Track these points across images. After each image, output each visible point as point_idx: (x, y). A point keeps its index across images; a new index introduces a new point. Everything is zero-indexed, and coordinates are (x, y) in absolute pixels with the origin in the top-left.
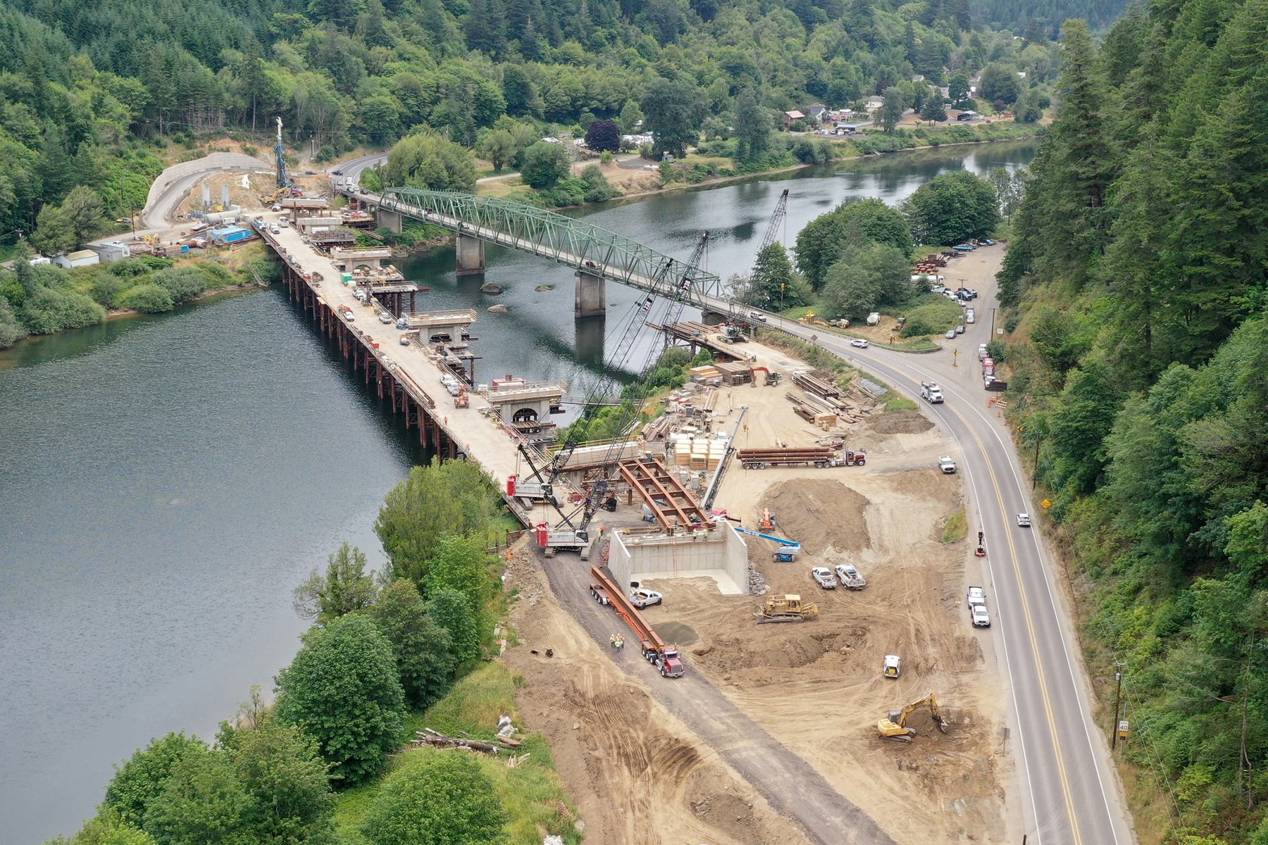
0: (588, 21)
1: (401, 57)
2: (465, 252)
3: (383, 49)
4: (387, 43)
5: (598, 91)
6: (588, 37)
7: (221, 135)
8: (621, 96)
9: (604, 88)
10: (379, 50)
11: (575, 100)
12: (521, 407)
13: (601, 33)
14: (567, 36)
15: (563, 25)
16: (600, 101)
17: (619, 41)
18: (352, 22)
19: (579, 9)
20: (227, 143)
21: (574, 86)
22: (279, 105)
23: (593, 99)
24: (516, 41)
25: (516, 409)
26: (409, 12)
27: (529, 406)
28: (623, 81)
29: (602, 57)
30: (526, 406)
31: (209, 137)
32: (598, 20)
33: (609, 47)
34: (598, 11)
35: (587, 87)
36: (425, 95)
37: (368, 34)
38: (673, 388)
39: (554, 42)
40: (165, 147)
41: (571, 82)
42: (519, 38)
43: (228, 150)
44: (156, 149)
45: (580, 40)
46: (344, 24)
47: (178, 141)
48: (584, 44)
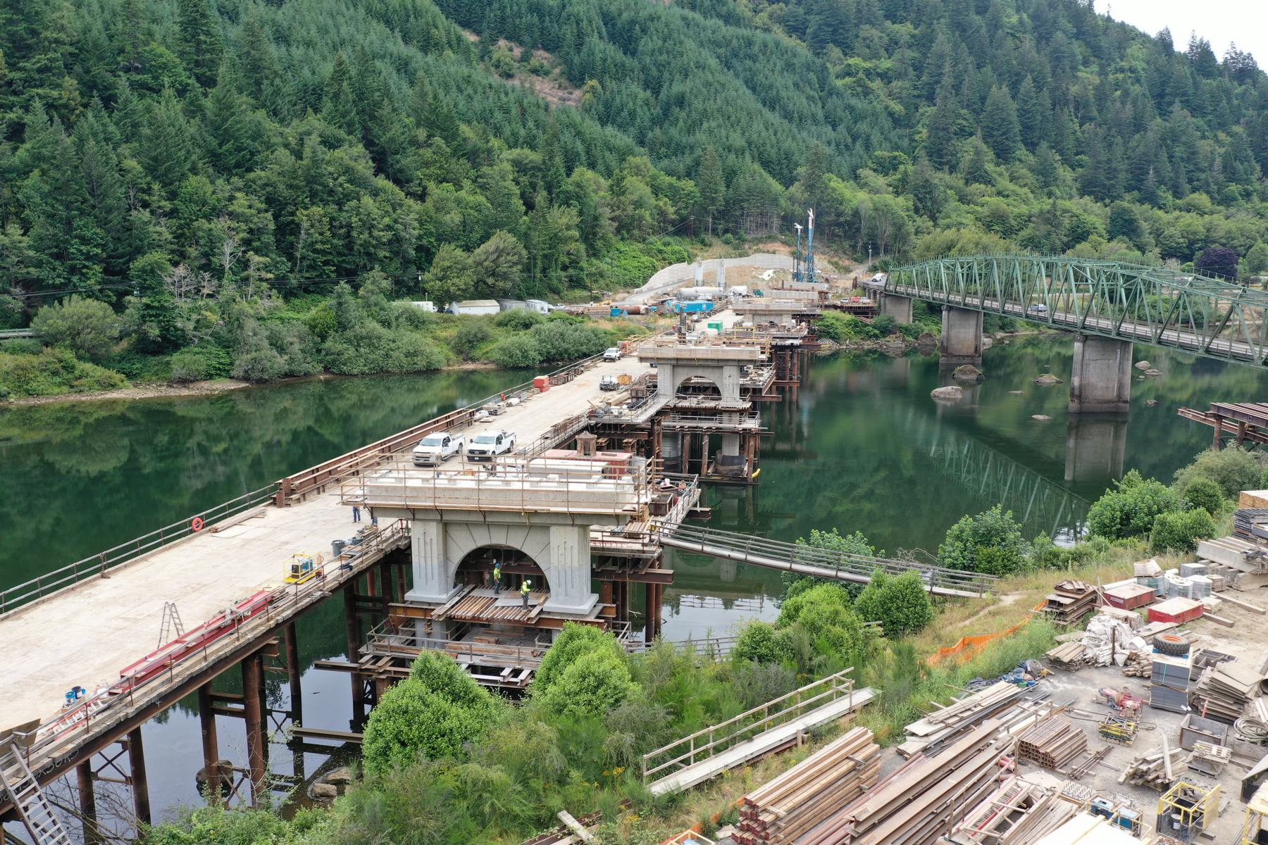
0: (1221, 177)
1: (999, 193)
2: (953, 333)
3: (983, 186)
4: (989, 182)
5: (1222, 233)
6: (1218, 192)
7: (771, 239)
8: (1248, 242)
9: (1229, 232)
10: (977, 187)
11: (1191, 243)
12: (482, 539)
13: (1234, 188)
14: (1194, 190)
15: (1190, 181)
16: (1224, 245)
17: (1255, 198)
18: (954, 162)
19: (1211, 166)
20: (776, 246)
21: (1193, 229)
22: (839, 215)
23: (1214, 242)
24: (1136, 193)
25: (464, 544)
26: (1020, 160)
27: (515, 541)
28: (1254, 228)
29: (1232, 210)
30: (499, 538)
31: (760, 241)
32: (1232, 176)
33: (1243, 202)
34: (1234, 168)
35: (1208, 230)
36: (1013, 223)
37: (969, 173)
38: (1159, 548)
39: (1178, 194)
40: (710, 246)
41: (1189, 225)
42: (1139, 190)
43: (774, 252)
44: (699, 246)
45: (1208, 193)
46: (946, 164)
47: (727, 243)
48: (1211, 197)
